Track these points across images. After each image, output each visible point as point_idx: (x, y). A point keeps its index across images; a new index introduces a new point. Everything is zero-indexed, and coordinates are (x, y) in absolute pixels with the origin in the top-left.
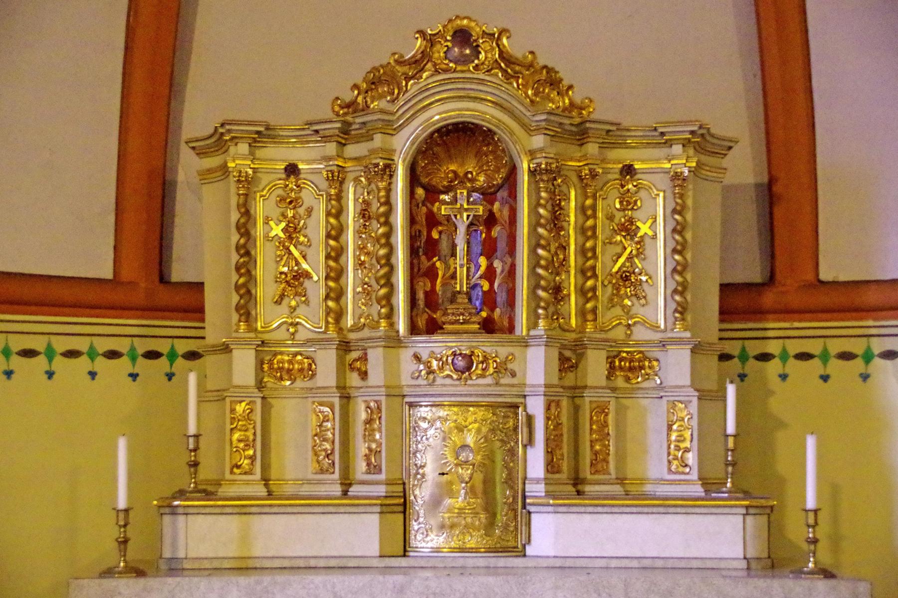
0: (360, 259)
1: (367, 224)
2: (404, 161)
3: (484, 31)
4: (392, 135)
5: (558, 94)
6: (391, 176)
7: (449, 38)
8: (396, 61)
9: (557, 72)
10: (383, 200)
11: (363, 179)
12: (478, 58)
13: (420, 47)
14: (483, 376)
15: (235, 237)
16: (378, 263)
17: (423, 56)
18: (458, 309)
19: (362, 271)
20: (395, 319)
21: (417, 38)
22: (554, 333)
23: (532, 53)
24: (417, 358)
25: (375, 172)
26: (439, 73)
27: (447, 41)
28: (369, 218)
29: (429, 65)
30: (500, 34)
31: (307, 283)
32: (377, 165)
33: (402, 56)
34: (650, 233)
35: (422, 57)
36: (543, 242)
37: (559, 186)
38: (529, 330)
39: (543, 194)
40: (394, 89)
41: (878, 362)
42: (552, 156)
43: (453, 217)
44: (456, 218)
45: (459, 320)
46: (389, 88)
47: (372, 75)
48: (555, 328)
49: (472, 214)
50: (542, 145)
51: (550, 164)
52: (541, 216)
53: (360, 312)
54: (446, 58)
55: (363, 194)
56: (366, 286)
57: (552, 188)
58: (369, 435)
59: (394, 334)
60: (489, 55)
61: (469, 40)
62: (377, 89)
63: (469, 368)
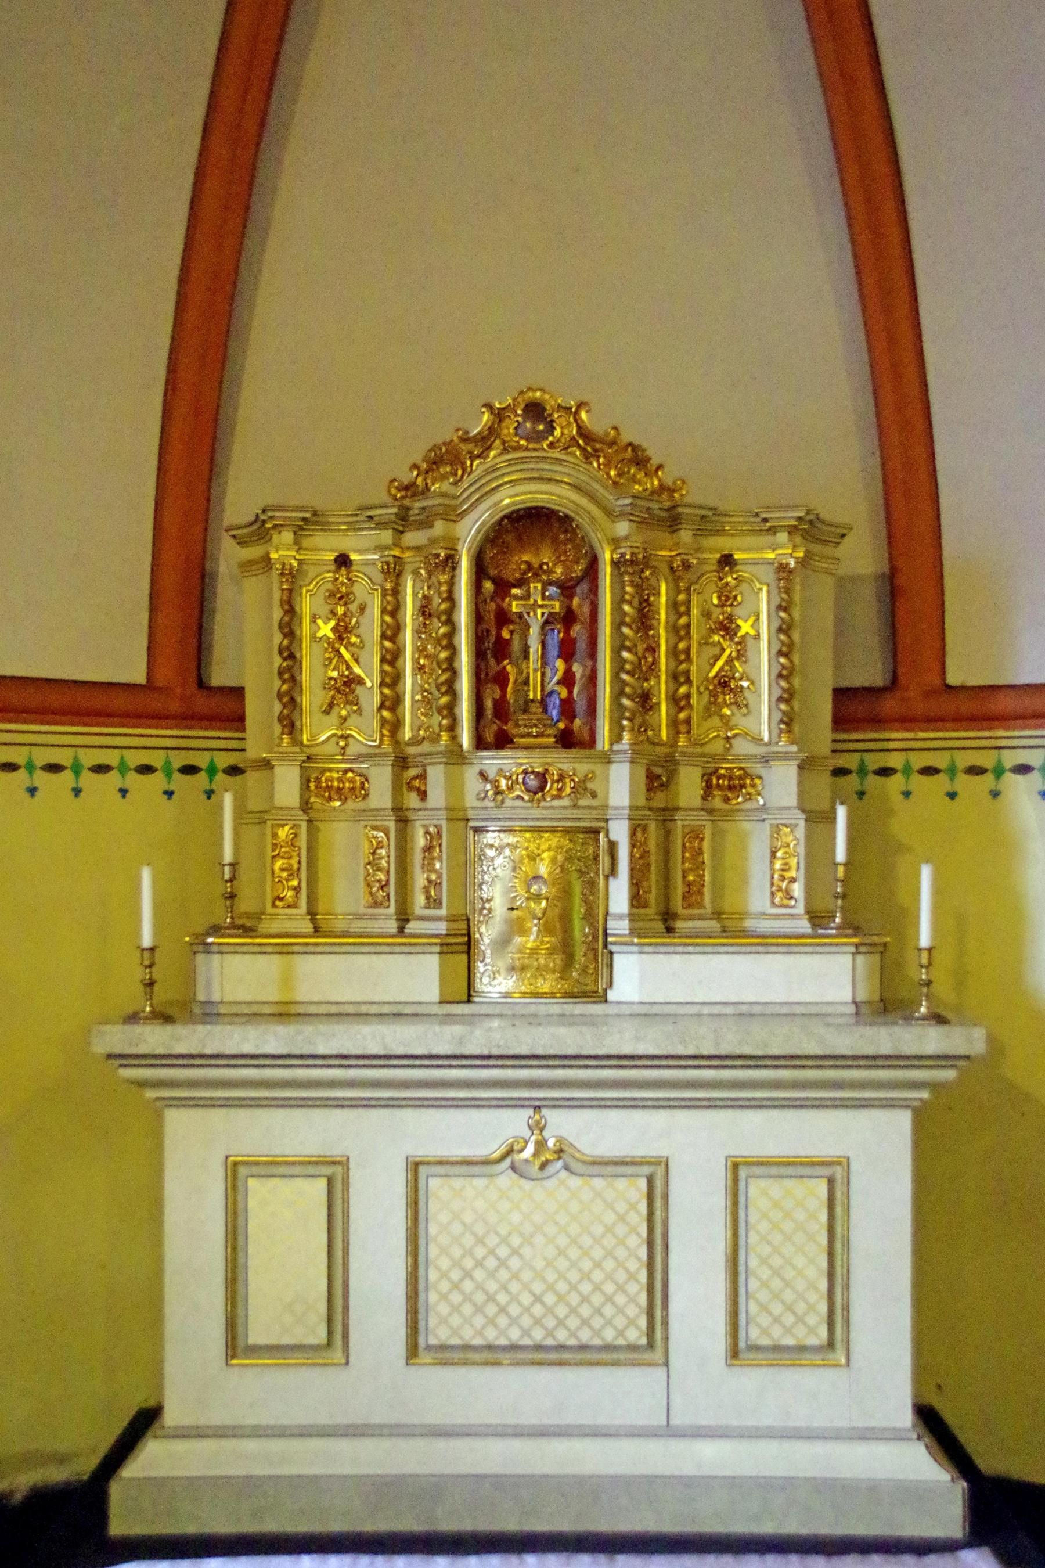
0: (419, 663)
1: (427, 622)
4: (455, 521)
5: (646, 474)
6: (454, 569)
10: (445, 595)
11: (423, 572)
14: (558, 797)
15: (278, 638)
19: (422, 677)
20: (459, 730)
23: (615, 428)
24: (483, 775)
27: (517, 415)
28: (430, 615)
29: (498, 442)
31: (359, 690)
32: (438, 556)
33: (467, 432)
34: (752, 632)
38: (611, 745)
39: (628, 589)
40: (457, 470)
41: (1009, 777)
46: (452, 468)
48: (641, 742)
54: (516, 434)
55: (422, 588)
56: (425, 694)
58: (428, 865)
60: (566, 431)
62: (438, 469)
63: (542, 788)
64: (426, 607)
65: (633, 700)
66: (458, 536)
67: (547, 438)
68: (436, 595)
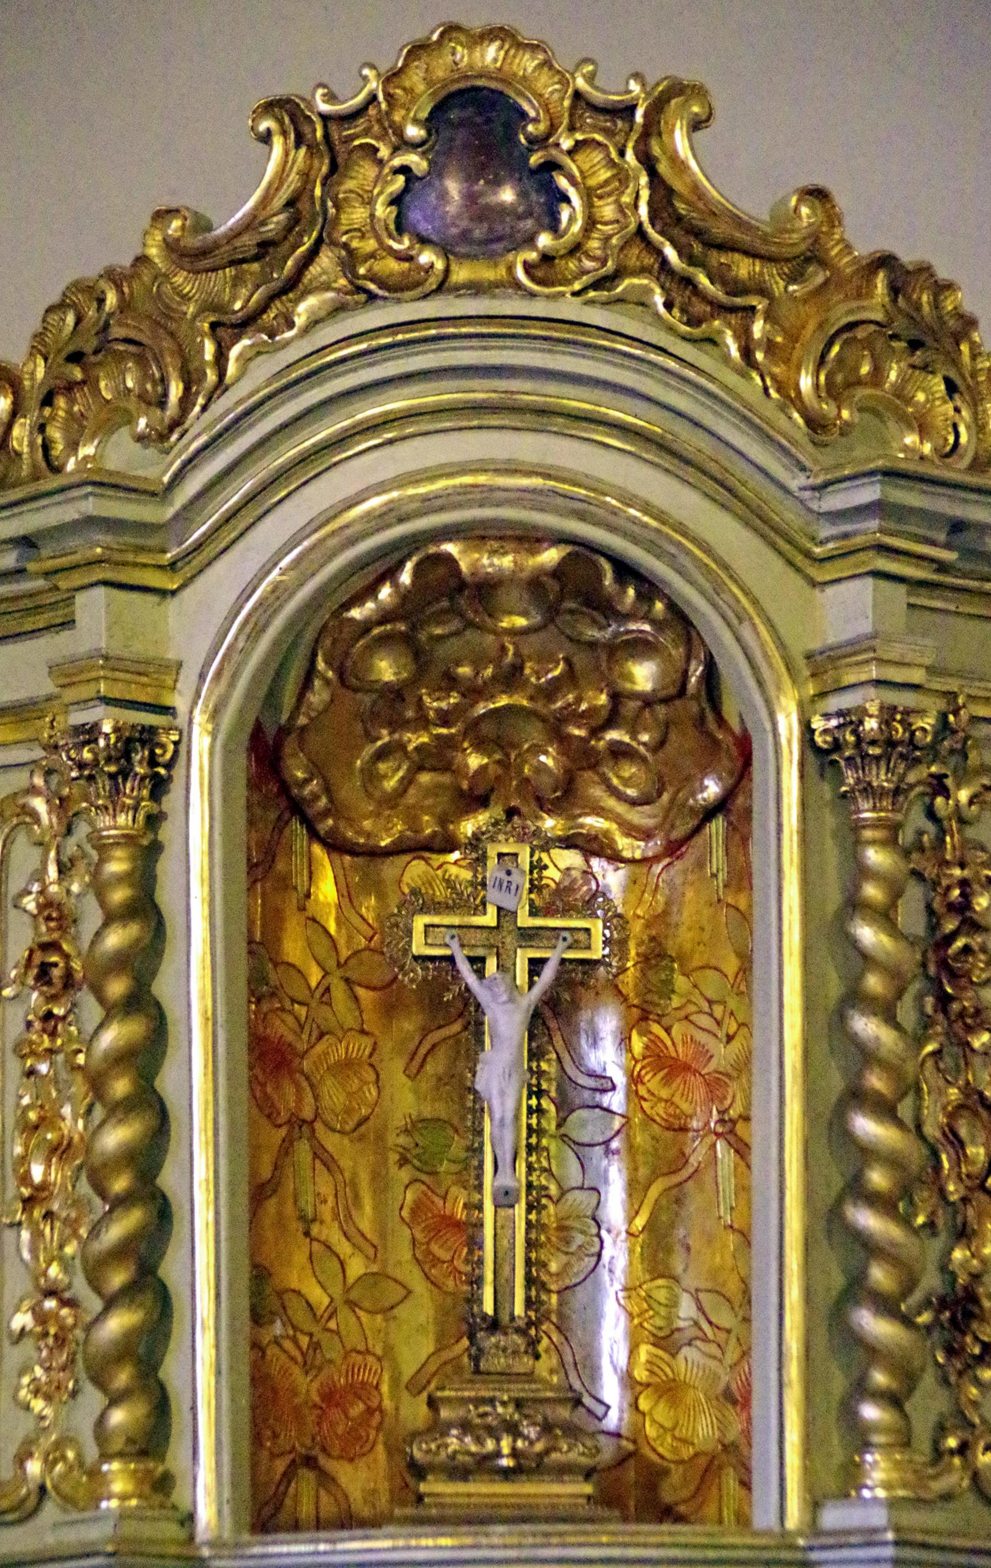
0: (26, 1179)
1: (59, 1011)
2: (215, 715)
3: (577, 95)
4: (163, 593)
5: (951, 388)
6: (159, 787)
7: (414, 132)
8: (170, 246)
9: (942, 288)
10: (119, 895)
11: (39, 804)
12: (554, 227)
13: (281, 176)
16: (102, 1192)
17: (295, 220)
18: (491, 1401)
19: (37, 1235)
20: (176, 1457)
21: (266, 138)
22: (936, 1519)
23: (818, 195)
25: (81, 765)
26: (372, 297)
27: (403, 145)
28: (69, 982)
29: (326, 260)
30: (658, 107)
32: (89, 733)
33: (202, 225)
35: (289, 229)
36: (876, 1081)
37: (962, 821)
38: (814, 1504)
39: (875, 857)
40: (164, 381)
42: (917, 676)
43: (464, 968)
44: (480, 973)
45: (498, 1454)
46: (145, 376)
47: (70, 319)
48: (947, 1497)
49: (553, 956)
50: (865, 627)
51: (907, 712)
52: (866, 959)
53: (26, 1426)
54: (401, 227)
55: (39, 875)
56: (50, 1304)
57: (930, 827)
59: (172, 1530)
60: (607, 211)
61: (511, 138)
62: (90, 382)
64: (48, 947)
65: (907, 1321)
66: (171, 655)
67: (530, 241)
68: (91, 904)
